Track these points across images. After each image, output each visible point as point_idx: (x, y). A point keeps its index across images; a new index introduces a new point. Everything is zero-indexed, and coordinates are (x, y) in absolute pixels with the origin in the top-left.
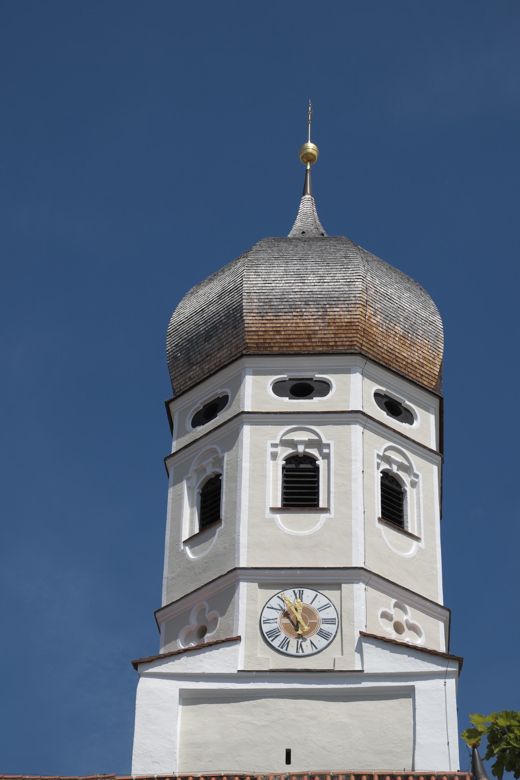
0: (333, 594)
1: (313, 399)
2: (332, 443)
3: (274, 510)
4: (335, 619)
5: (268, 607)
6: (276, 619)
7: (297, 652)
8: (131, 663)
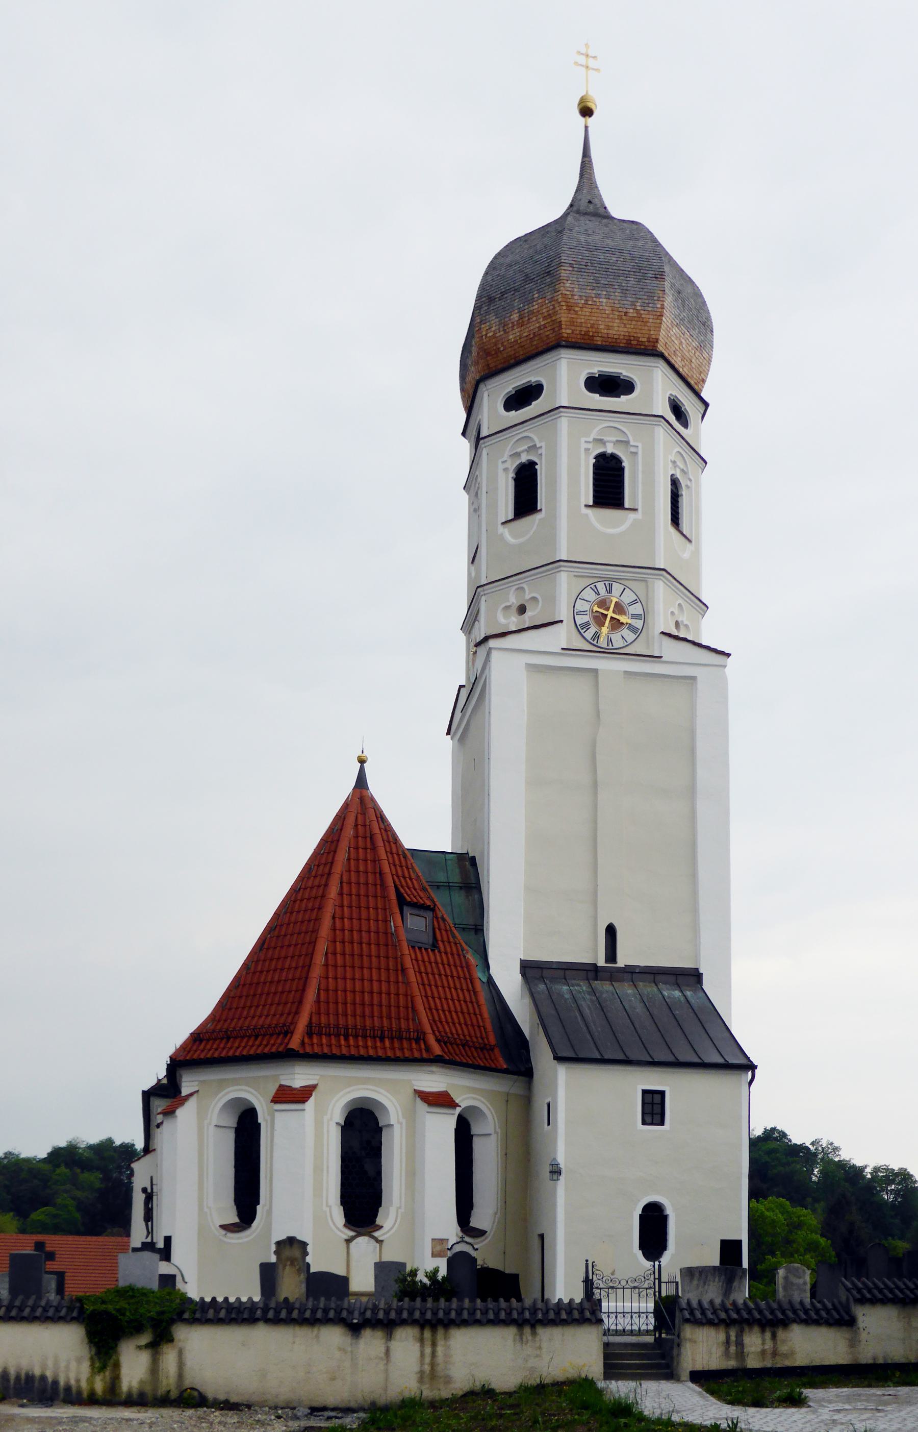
0: (639, 587)
1: (620, 397)
2: (640, 445)
3: (587, 506)
4: (636, 600)
7: (608, 646)
8: (583, 93)
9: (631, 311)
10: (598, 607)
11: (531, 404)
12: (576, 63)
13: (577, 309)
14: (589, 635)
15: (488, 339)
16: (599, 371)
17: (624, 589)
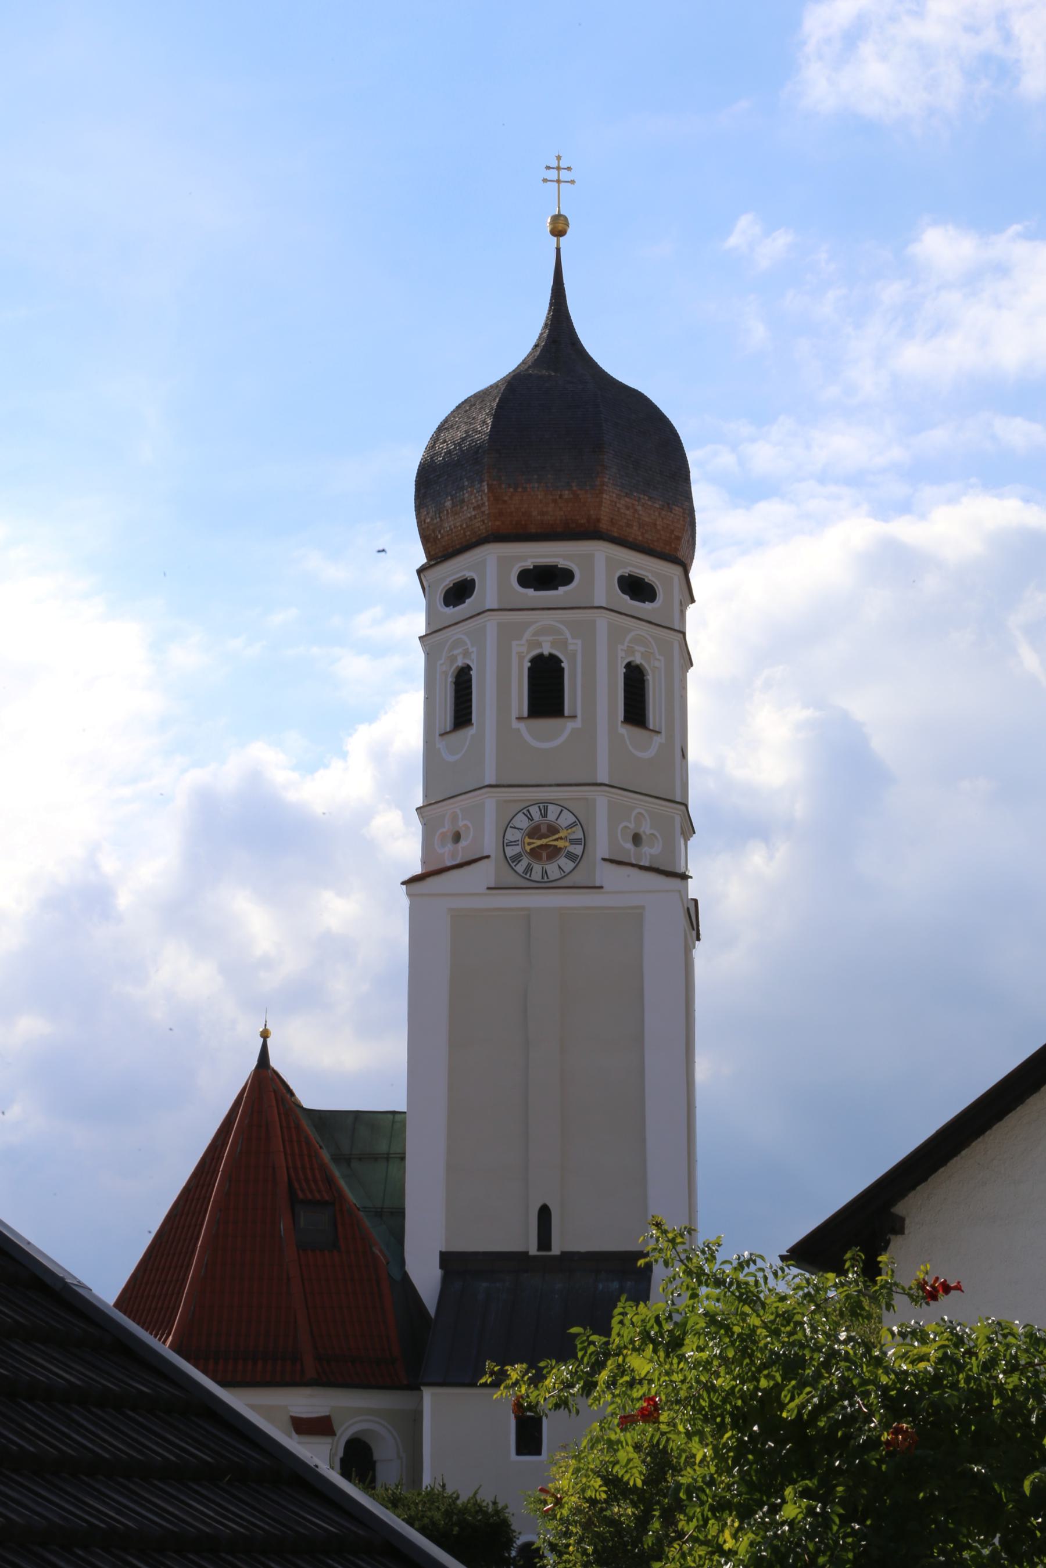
4: (575, 822)
5: (511, 827)
6: (518, 841)
9: (567, 492)
10: (529, 838)
11: (464, 602)
12: (545, 180)
13: (506, 498)
14: (520, 868)
15: (426, 525)
16: (532, 563)
17: (562, 810)
